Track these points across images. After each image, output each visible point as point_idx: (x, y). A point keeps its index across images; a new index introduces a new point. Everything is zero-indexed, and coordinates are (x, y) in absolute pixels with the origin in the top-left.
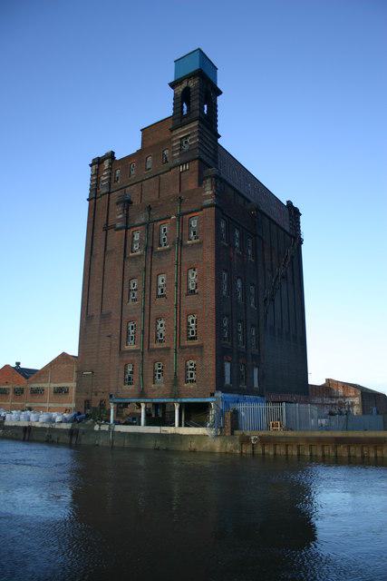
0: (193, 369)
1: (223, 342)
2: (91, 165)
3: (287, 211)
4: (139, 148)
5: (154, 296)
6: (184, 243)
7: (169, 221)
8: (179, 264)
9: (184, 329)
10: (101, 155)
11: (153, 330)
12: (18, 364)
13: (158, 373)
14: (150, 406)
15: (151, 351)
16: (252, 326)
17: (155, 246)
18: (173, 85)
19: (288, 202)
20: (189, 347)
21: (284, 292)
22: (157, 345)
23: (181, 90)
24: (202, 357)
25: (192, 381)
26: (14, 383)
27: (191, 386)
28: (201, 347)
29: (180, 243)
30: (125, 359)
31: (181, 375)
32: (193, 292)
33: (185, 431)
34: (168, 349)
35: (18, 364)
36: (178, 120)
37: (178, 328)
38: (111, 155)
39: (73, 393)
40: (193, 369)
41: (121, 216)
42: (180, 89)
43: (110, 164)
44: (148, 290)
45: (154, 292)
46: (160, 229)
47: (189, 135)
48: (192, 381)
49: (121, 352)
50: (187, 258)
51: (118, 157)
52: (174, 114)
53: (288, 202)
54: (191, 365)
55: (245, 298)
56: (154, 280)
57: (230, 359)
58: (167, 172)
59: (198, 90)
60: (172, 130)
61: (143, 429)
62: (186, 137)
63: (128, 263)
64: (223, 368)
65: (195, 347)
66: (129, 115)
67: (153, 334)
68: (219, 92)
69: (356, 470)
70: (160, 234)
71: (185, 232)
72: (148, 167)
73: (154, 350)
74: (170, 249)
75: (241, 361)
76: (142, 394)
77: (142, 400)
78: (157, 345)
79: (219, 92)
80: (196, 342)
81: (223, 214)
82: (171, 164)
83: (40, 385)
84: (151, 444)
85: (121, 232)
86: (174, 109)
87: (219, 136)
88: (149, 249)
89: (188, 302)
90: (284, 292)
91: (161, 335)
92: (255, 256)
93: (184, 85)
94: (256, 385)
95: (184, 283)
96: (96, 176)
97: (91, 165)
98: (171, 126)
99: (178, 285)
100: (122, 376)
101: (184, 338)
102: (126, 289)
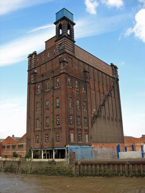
0: (59, 137)
1: (78, 126)
2: (28, 57)
3: (111, 68)
4: (45, 49)
5: (45, 109)
6: (55, 88)
7: (49, 80)
8: (53, 96)
9: (55, 121)
10: (31, 53)
11: (45, 122)
12: (13, 136)
13: (47, 138)
14: (57, 151)
15: (44, 130)
16: (85, 118)
17: (45, 90)
18: (55, 23)
19: (111, 64)
20: (57, 128)
21: (110, 102)
22: (47, 128)
23: (58, 25)
24: (61, 131)
25: (59, 141)
26: (11, 142)
27: (58, 143)
28: (61, 128)
29: (53, 88)
30: (36, 134)
31: (54, 139)
32: (58, 107)
33: (56, 160)
34: (50, 129)
35: (13, 136)
36: (58, 37)
37: (53, 121)
38: (35, 53)
39: (25, 148)
40: (59, 137)
41: (33, 79)
42: (58, 25)
43: (35, 56)
44: (43, 107)
45: (45, 107)
46: (46, 83)
47: (62, 43)
48: (59, 141)
49: (34, 131)
50: (56, 94)
51: (38, 53)
52: (56, 35)
53: (111, 64)
54: (58, 135)
55: (81, 108)
56: (45, 103)
57: (73, 132)
58: (54, 58)
59: (65, 24)
60: (56, 41)
61: (42, 160)
62: (61, 44)
63: (36, 96)
64: (70, 136)
65: (59, 128)
66: (39, 39)
67: (45, 124)
68: (74, 24)
69: (11, 175)
70: (46, 85)
71: (55, 84)
72: (48, 57)
73: (56, 128)
74: (50, 91)
75: (79, 132)
76: (42, 147)
77: (42, 149)
78: (47, 128)
79: (74, 24)
80: (59, 126)
81: (68, 75)
82: (56, 55)
83: (22, 144)
84: (44, 166)
85: (33, 85)
86: (56, 33)
87: (75, 42)
88: (42, 91)
89: (57, 111)
90: (110, 102)
91: (48, 124)
92: (86, 90)
93: (60, 23)
94: (87, 141)
95: (55, 103)
96: (30, 61)
97: (28, 57)
98: (80, 31)
99: (53, 104)
100: (35, 140)
101: (55, 124)
102: (35, 107)
